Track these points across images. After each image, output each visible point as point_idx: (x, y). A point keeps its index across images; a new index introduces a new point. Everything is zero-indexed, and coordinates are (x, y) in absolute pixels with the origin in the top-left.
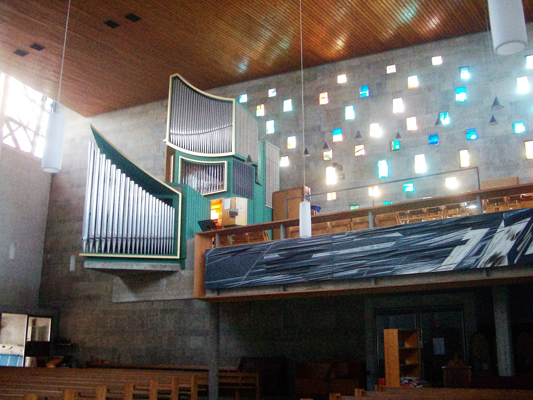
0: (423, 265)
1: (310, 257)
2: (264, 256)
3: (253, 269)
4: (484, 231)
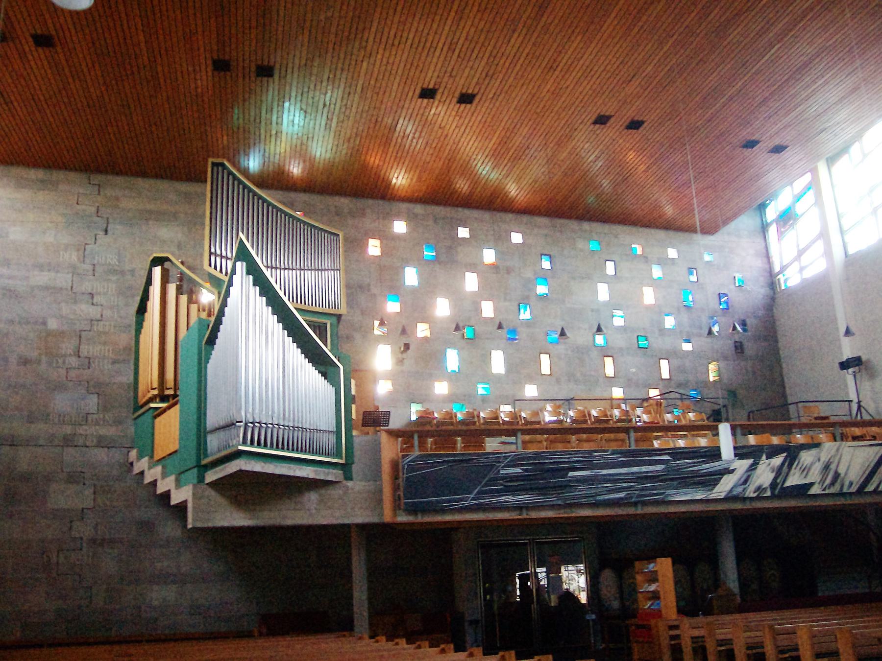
0: (696, 491)
1: (566, 475)
2: (499, 471)
3: (483, 487)
4: (750, 461)
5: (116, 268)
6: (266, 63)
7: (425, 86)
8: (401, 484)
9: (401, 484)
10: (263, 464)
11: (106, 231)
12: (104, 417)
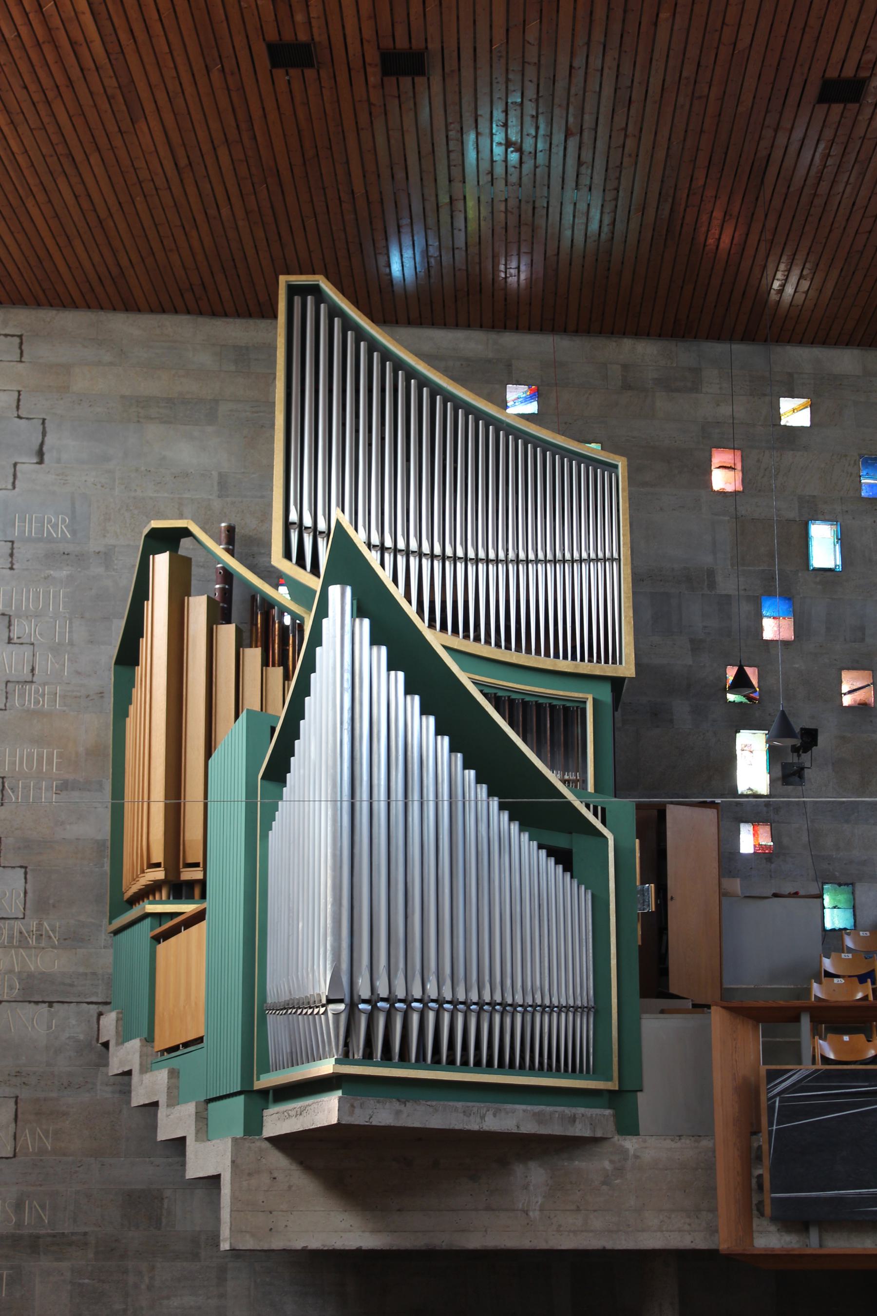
5: (70, 548)
6: (402, 43)
7: (832, 73)
8: (765, 1147)
9: (765, 1147)
10: (397, 1106)
11: (40, 454)
12: (40, 925)
